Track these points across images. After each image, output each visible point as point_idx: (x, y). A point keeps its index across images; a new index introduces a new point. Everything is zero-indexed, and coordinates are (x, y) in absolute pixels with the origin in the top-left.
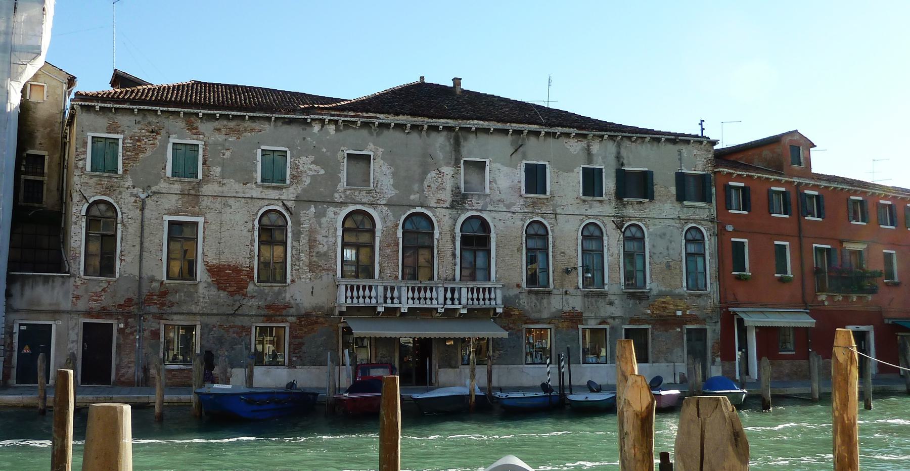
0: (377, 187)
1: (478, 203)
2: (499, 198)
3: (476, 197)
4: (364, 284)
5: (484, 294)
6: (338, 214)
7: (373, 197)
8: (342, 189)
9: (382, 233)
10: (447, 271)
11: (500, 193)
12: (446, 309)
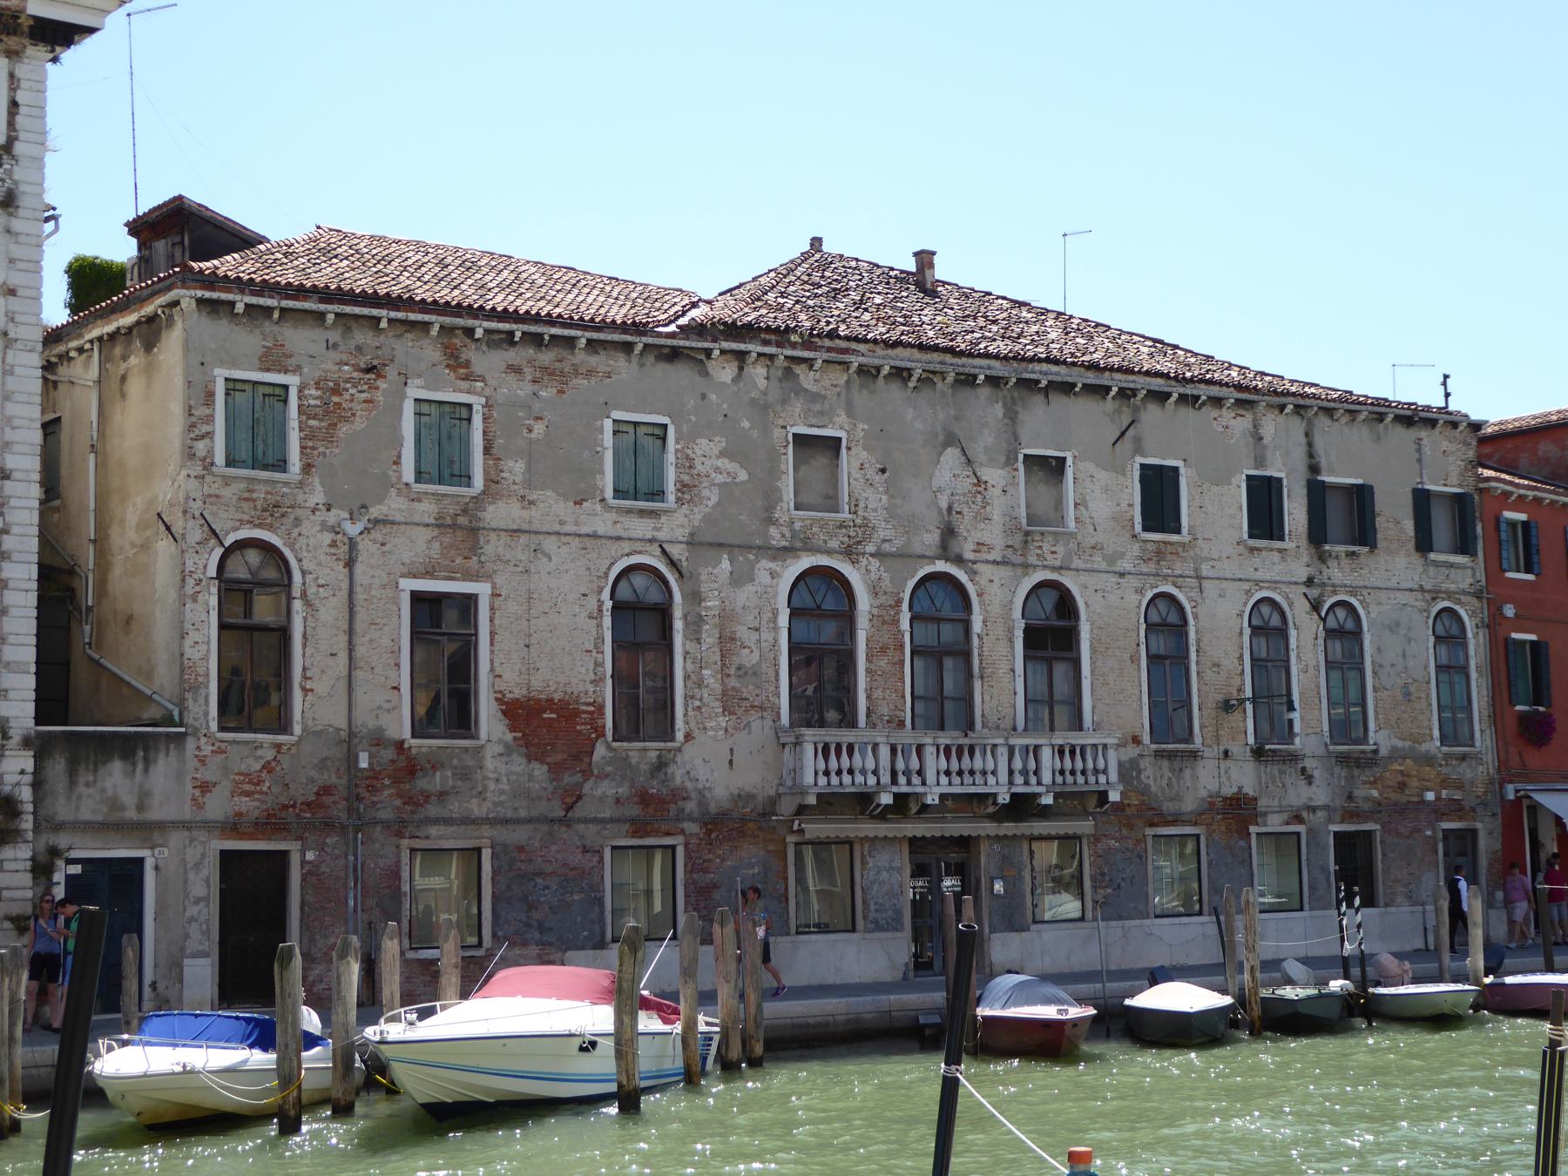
2: (1093, 541)
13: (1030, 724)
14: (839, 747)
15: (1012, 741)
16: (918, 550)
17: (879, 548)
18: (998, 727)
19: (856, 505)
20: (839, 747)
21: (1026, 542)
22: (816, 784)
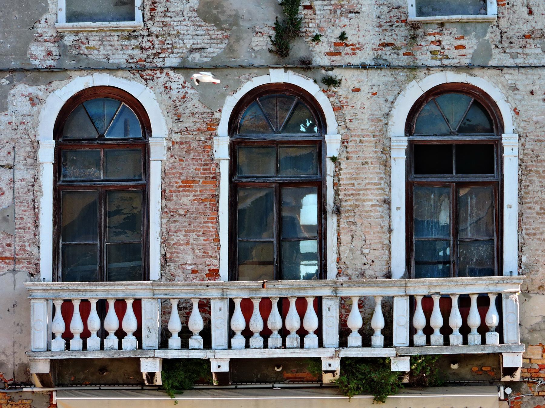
0: (152, 18)
1: (463, 47)
2: (526, 29)
3: (454, 31)
4: (102, 295)
5: (465, 315)
6: (41, 101)
7: (142, 48)
8: (50, 33)
9: (169, 149)
10: (366, 251)
11: (530, 13)
12: (344, 361)
13: (413, 269)
14: (85, 305)
15: (344, 292)
16: (244, 57)
17: (185, 59)
18: (362, 274)
19: (153, 10)
20: (85, 305)
21: (414, 37)
22: (48, 350)
